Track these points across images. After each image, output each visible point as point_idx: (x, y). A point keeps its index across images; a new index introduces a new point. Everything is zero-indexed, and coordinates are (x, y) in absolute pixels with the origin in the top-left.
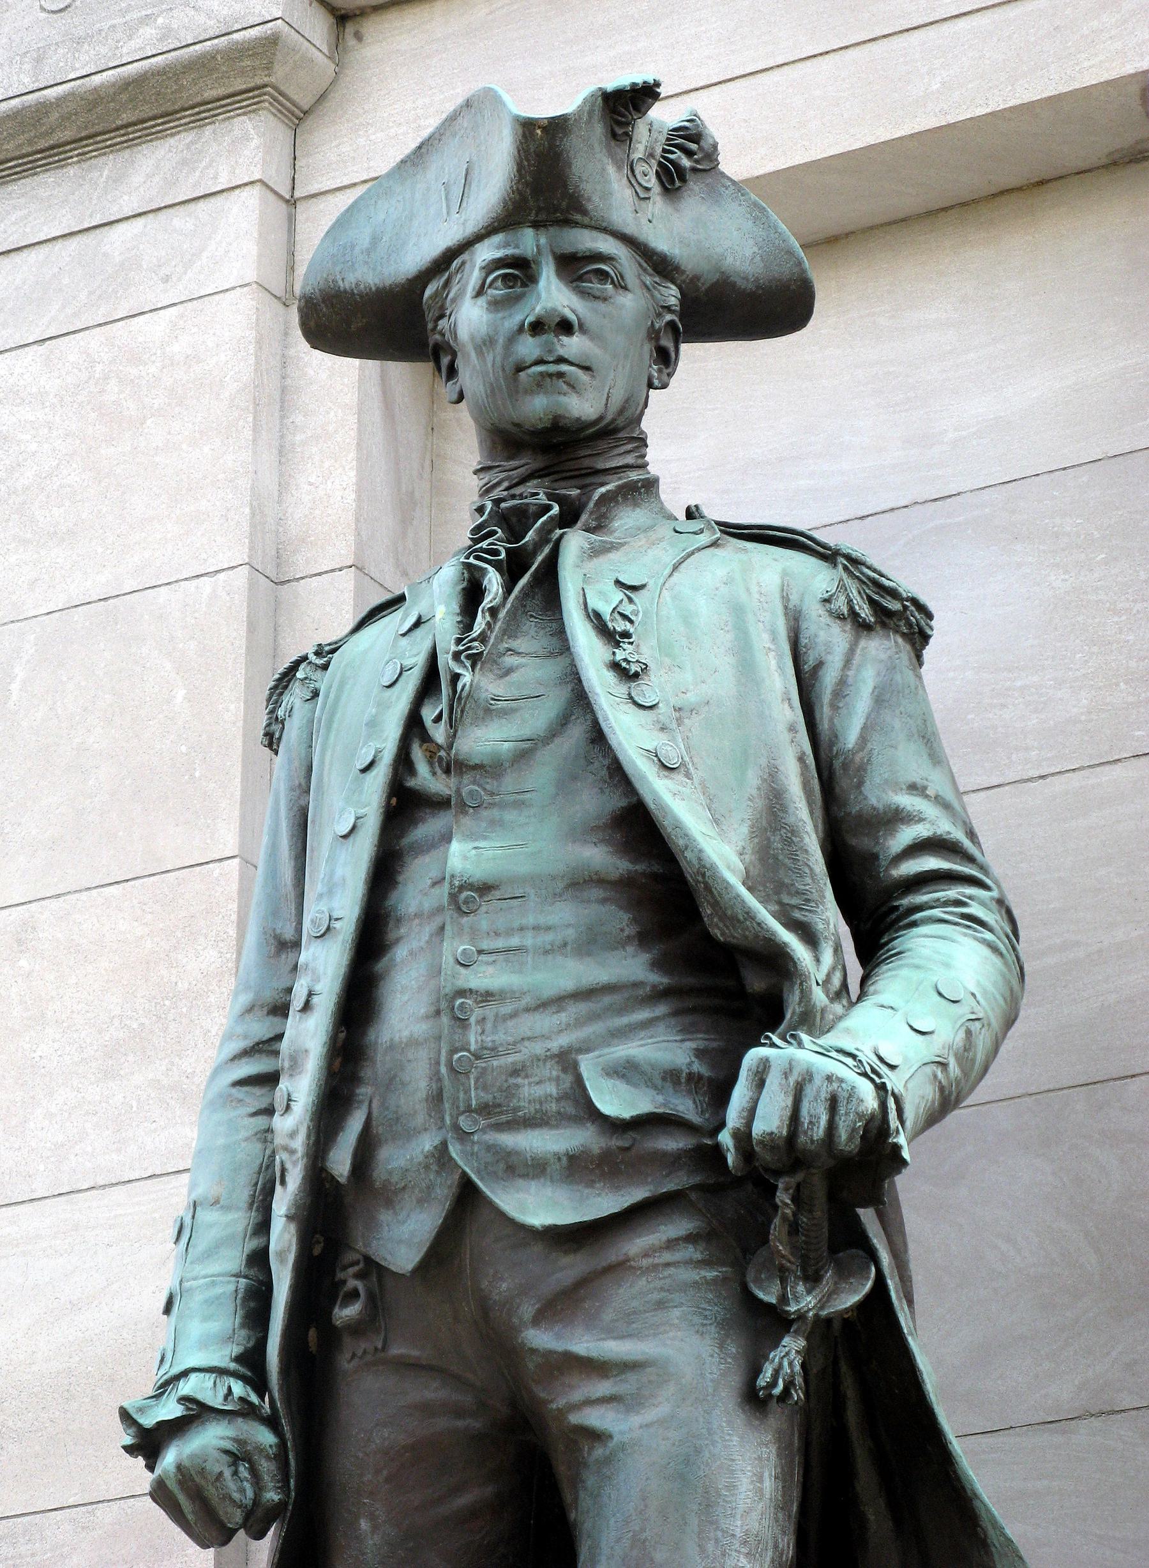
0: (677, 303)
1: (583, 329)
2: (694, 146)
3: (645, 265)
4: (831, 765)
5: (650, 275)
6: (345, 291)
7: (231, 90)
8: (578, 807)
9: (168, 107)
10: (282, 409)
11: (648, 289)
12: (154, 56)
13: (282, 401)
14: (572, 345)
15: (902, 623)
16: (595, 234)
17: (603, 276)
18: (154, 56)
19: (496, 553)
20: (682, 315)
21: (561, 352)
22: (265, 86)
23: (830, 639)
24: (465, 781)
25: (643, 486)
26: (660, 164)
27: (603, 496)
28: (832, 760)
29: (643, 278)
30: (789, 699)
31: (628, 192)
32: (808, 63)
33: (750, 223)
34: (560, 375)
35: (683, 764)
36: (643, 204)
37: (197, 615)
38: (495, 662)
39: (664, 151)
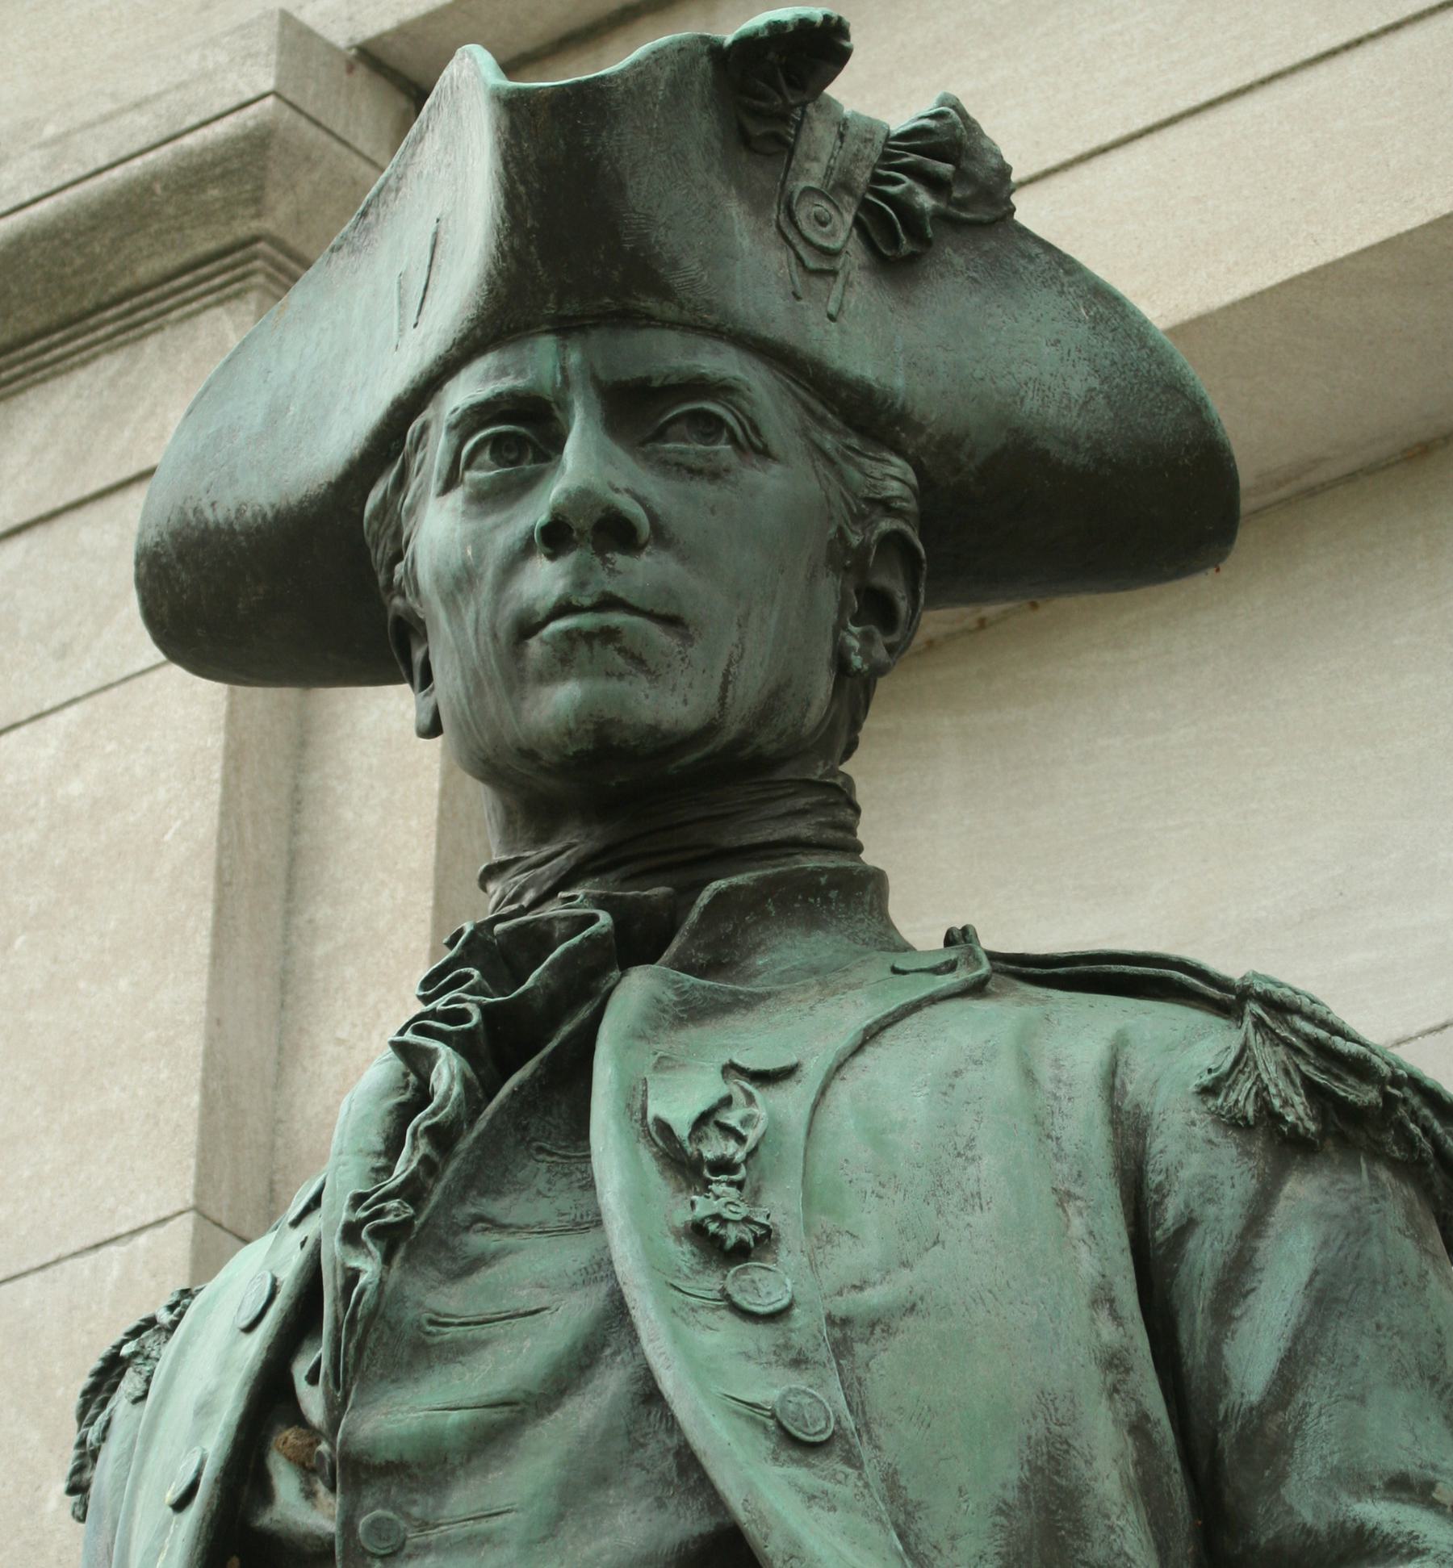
0: (907, 492)
1: (661, 535)
2: (945, 168)
3: (820, 409)
4: (1215, 1442)
5: (832, 430)
6: (218, 529)
7: (187, 256)
8: (606, 1541)
9: (67, 306)
10: (290, 894)
11: (830, 461)
12: (35, 201)
13: (290, 879)
14: (640, 572)
15: (1389, 1137)
16: (692, 339)
17: (709, 426)
18: (35, 201)
19: (464, 1016)
20: (926, 523)
21: (613, 586)
22: (256, 239)
23: (1200, 1166)
24: (368, 1501)
25: (831, 885)
26: (865, 205)
27: (719, 896)
28: (1216, 1433)
29: (816, 436)
30: (1112, 1301)
31: (777, 259)
32: (1323, 69)
33: (1083, 330)
34: (609, 635)
35: (838, 1435)
36: (818, 284)
37: (92, 1326)
38: (443, 1244)
39: (876, 179)
